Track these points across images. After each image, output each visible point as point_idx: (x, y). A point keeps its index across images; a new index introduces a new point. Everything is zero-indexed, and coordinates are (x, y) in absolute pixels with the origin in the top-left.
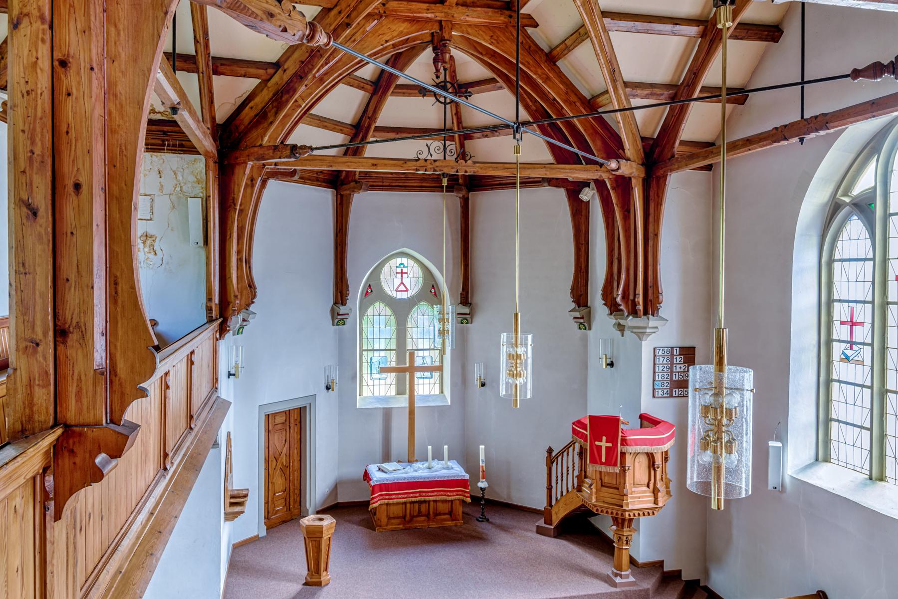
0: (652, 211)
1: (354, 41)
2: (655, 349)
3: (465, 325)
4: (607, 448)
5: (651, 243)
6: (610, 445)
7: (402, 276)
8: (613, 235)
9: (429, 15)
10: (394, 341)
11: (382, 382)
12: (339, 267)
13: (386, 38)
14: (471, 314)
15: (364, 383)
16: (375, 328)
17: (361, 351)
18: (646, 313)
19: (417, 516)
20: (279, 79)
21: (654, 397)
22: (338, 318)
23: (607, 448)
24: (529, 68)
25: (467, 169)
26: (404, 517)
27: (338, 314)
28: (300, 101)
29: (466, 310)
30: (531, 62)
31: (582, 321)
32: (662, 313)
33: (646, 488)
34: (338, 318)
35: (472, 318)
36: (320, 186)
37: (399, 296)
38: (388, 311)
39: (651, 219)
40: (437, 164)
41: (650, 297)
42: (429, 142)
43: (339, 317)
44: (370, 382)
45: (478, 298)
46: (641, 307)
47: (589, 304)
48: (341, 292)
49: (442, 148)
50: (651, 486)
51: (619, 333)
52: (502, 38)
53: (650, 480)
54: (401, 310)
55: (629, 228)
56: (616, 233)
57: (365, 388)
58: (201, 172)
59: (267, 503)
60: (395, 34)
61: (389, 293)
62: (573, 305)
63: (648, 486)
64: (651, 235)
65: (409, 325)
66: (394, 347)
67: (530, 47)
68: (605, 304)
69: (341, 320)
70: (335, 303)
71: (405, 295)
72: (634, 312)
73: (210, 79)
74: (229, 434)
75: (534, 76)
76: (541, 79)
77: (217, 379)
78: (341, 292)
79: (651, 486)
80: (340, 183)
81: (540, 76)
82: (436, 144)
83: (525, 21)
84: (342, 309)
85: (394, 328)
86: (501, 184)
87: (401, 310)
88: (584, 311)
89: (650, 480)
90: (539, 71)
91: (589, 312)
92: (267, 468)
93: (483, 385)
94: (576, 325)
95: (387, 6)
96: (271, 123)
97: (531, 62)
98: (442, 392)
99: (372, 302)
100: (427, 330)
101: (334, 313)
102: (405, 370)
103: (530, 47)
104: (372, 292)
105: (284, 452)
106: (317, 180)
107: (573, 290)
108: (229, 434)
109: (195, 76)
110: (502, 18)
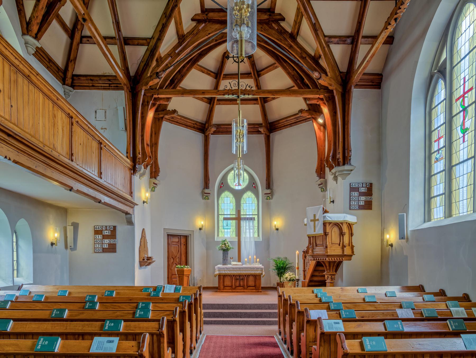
0: (346, 110)
7: (238, 178)
10: (234, 210)
11: (229, 230)
13: (209, 32)
14: (272, 194)
15: (220, 231)
16: (226, 203)
18: (344, 164)
19: (238, 287)
20: (152, 43)
21: (350, 209)
24: (281, 42)
26: (231, 286)
27: (205, 193)
29: (268, 191)
30: (282, 39)
31: (321, 186)
32: (352, 162)
33: (338, 246)
35: (272, 196)
36: (195, 131)
37: (237, 188)
38: (231, 196)
39: (346, 114)
41: (346, 155)
42: (230, 81)
44: (223, 230)
46: (341, 160)
48: (206, 183)
49: (237, 84)
50: (341, 244)
51: (335, 182)
52: (267, 27)
53: (340, 241)
54: (238, 195)
57: (220, 233)
59: (168, 278)
60: (213, 30)
61: (232, 186)
62: (318, 178)
63: (339, 245)
64: (346, 122)
65: (242, 202)
66: (234, 213)
67: (281, 31)
69: (207, 196)
70: (204, 189)
71: (240, 188)
72: (339, 165)
75: (284, 46)
76: (288, 47)
77: (132, 193)
78: (206, 183)
79: (341, 244)
81: (287, 46)
83: (278, 17)
84: (206, 191)
85: (234, 204)
86: (285, 126)
87: (238, 195)
89: (340, 241)
90: (287, 43)
92: (168, 261)
95: (209, 15)
97: (282, 39)
99: (223, 191)
100: (250, 204)
103: (281, 31)
104: (224, 186)
105: (178, 256)
106: (194, 128)
109: (116, 46)
110: (266, 16)
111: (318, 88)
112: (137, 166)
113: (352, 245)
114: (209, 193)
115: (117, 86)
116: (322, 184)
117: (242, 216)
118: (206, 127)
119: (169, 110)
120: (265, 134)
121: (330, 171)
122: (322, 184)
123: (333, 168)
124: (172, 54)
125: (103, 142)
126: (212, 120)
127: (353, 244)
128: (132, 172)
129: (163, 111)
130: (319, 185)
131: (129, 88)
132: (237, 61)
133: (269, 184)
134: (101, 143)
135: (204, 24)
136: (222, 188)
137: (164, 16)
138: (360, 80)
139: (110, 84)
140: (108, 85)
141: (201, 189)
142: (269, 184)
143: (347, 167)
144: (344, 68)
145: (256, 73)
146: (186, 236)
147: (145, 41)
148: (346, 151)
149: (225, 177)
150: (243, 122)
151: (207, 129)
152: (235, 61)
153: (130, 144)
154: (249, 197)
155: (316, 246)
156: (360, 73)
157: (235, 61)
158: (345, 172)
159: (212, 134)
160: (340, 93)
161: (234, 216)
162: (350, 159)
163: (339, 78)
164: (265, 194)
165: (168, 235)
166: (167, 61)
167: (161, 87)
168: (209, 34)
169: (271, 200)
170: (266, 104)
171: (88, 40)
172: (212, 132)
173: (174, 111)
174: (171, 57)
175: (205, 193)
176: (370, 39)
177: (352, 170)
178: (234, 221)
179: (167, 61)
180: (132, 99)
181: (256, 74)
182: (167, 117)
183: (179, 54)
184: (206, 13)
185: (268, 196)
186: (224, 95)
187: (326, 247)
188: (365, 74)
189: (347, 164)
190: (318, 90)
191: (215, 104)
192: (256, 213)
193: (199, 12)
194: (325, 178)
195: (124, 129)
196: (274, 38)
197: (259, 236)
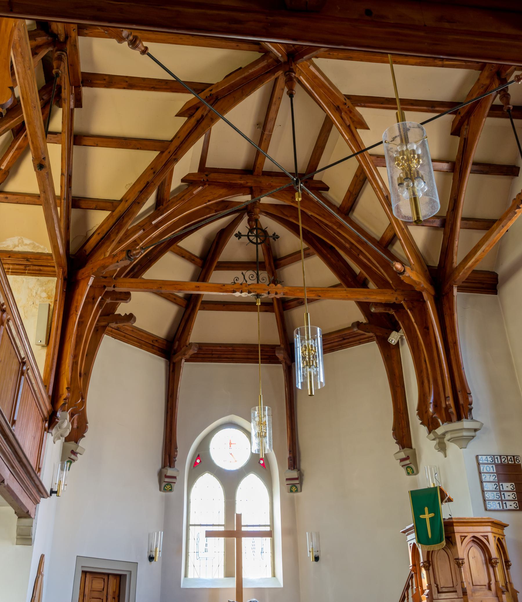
1: (183, 200)
2: (477, 457)
3: (296, 494)
4: (424, 514)
5: (452, 352)
6: (432, 515)
7: (232, 446)
8: (419, 358)
9: (242, 182)
12: (168, 430)
13: (208, 198)
14: (300, 478)
16: (204, 499)
17: (188, 526)
18: (459, 419)
20: (120, 209)
22: (166, 482)
23: (424, 514)
25: (279, 292)
27: (167, 477)
28: (138, 241)
29: (294, 474)
31: (408, 462)
32: (474, 413)
34: (166, 482)
35: (301, 484)
39: (448, 331)
40: (251, 287)
41: (461, 401)
42: (244, 272)
43: (167, 480)
45: (306, 464)
46: (453, 410)
47: (414, 446)
51: (441, 454)
54: (230, 481)
55: (431, 343)
56: (423, 356)
58: (52, 290)
60: (216, 196)
62: (397, 447)
63: (490, 589)
64: (451, 345)
66: (223, 523)
68: (421, 424)
69: (169, 483)
70: (164, 466)
72: (449, 420)
73: (72, 111)
74: (42, 556)
76: (336, 226)
79: (493, 586)
80: (171, 349)
82: (249, 273)
84: (170, 472)
87: (230, 481)
88: (408, 451)
89: (490, 580)
91: (414, 454)
93: (317, 559)
94: (403, 471)
96: (113, 241)
98: (274, 575)
100: (257, 501)
101: (161, 476)
102: (233, 533)
104: (202, 463)
107: (394, 429)
108: (42, 556)
111: (393, 289)
112: (59, 414)
113: (512, 589)
114: (175, 477)
115: (40, 270)
116: (407, 458)
117: (244, 529)
118: (175, 348)
119: (120, 315)
120: (286, 363)
121: (430, 432)
122: (407, 458)
123: (437, 426)
124: (146, 226)
125: (28, 362)
126: (189, 335)
127: (516, 587)
128: (47, 425)
129: (108, 315)
130: (402, 460)
131: (66, 273)
132: (255, 241)
133: (294, 461)
134: (24, 363)
135: (201, 188)
136: (197, 467)
137: (152, 171)
138: (467, 279)
139: (26, 266)
140: (22, 267)
141: (159, 466)
142: (294, 461)
143: (466, 424)
144: (435, 262)
145: (272, 263)
146: (120, 576)
147: (108, 204)
148: (460, 394)
149: (205, 443)
150: (314, 332)
151: (175, 352)
152: (251, 241)
153: (51, 370)
154: (252, 486)
155: (439, 592)
156: (470, 267)
157: (251, 241)
158: (465, 434)
159: (187, 361)
160: (432, 298)
161: (222, 529)
162: (470, 410)
163: (428, 272)
164: (287, 479)
165: (85, 573)
166: (137, 235)
167: (119, 275)
168: (209, 201)
169: (299, 494)
170: (285, 312)
171: (7, 198)
172: (187, 356)
173: (130, 317)
174: (144, 230)
175: (167, 477)
176: (471, 222)
177: (475, 430)
178: (222, 540)
179: (137, 235)
180: (66, 292)
181: (272, 264)
182: (113, 325)
183: (157, 226)
184: (206, 173)
185: (294, 485)
186: (234, 292)
187: (465, 593)
188: (474, 272)
189: (466, 418)
190: (394, 292)
191: (198, 307)
192: (484, 484)
193: (196, 171)
194: (411, 447)
195: (44, 343)
196: (314, 212)
197: (274, 575)
